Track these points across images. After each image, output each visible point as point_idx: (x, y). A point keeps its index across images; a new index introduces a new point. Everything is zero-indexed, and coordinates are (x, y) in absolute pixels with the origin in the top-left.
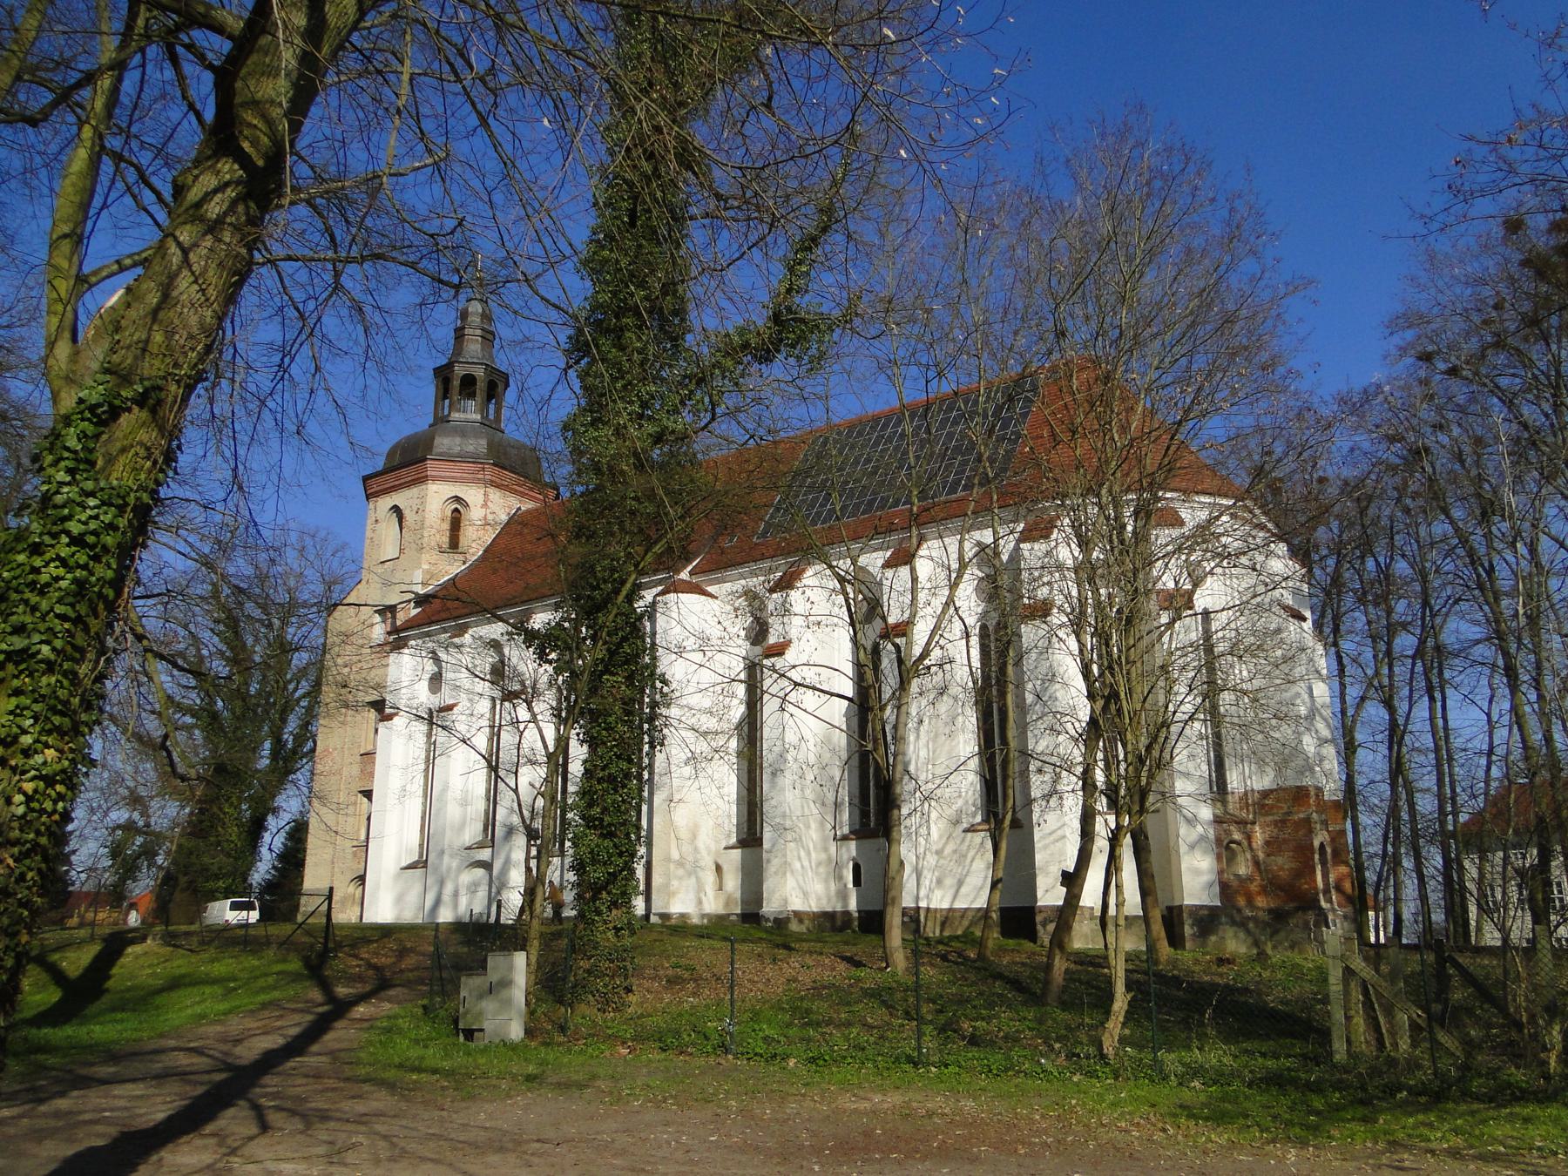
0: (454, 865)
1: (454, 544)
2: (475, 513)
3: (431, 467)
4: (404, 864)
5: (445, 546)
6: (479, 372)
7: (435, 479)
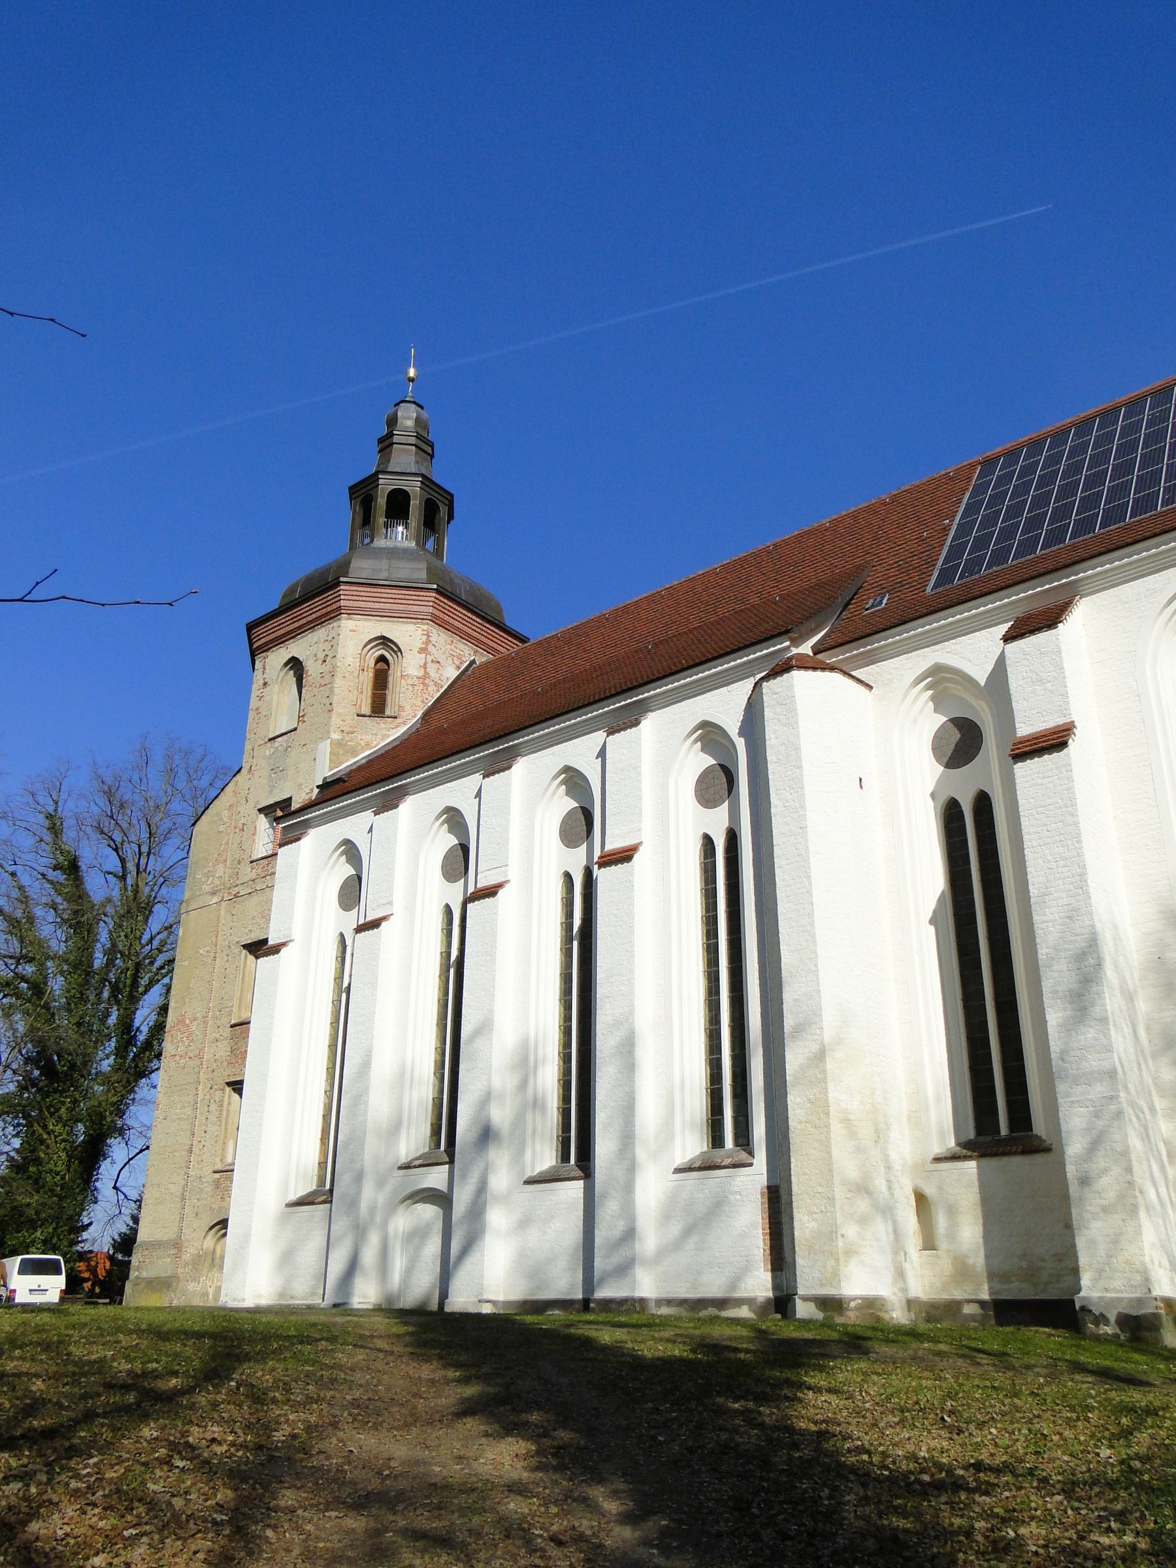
0: (381, 1199)
1: (378, 707)
2: (408, 666)
3: (347, 595)
4: (293, 1197)
5: (366, 710)
6: (414, 487)
7: (352, 612)
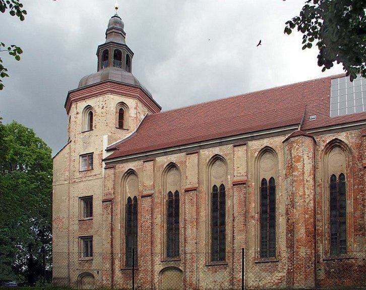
1: (121, 126)
5: (118, 126)
